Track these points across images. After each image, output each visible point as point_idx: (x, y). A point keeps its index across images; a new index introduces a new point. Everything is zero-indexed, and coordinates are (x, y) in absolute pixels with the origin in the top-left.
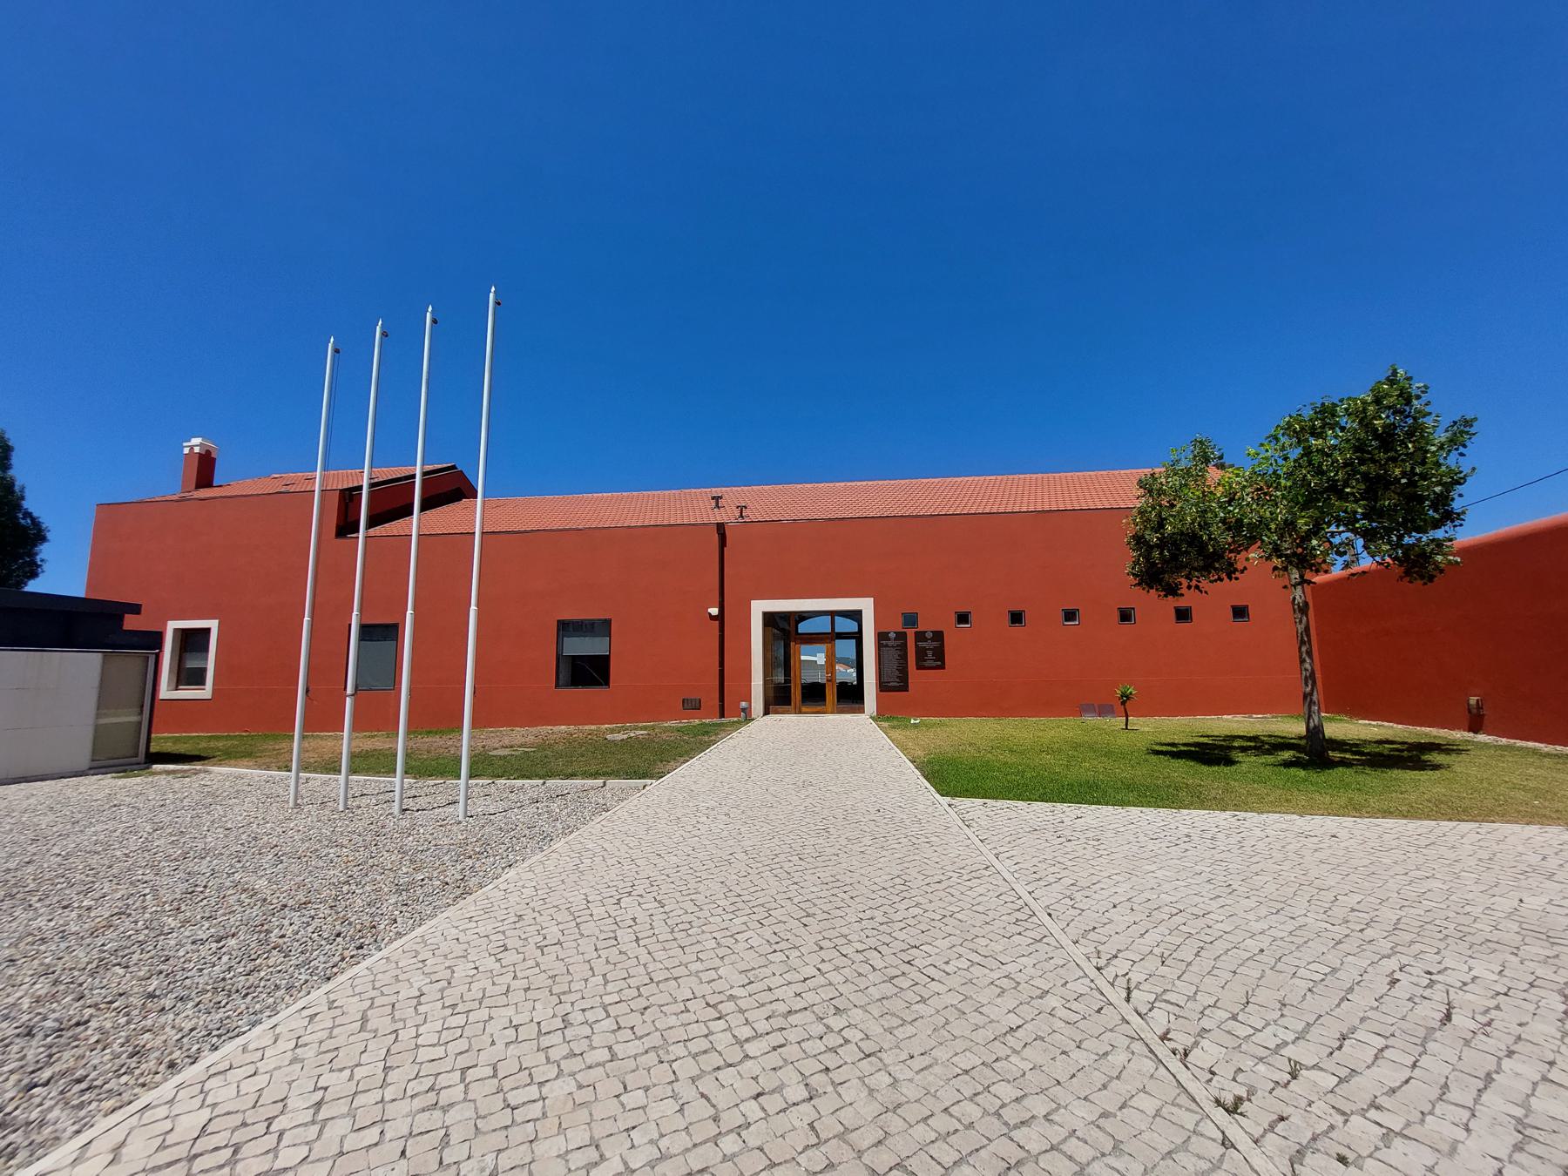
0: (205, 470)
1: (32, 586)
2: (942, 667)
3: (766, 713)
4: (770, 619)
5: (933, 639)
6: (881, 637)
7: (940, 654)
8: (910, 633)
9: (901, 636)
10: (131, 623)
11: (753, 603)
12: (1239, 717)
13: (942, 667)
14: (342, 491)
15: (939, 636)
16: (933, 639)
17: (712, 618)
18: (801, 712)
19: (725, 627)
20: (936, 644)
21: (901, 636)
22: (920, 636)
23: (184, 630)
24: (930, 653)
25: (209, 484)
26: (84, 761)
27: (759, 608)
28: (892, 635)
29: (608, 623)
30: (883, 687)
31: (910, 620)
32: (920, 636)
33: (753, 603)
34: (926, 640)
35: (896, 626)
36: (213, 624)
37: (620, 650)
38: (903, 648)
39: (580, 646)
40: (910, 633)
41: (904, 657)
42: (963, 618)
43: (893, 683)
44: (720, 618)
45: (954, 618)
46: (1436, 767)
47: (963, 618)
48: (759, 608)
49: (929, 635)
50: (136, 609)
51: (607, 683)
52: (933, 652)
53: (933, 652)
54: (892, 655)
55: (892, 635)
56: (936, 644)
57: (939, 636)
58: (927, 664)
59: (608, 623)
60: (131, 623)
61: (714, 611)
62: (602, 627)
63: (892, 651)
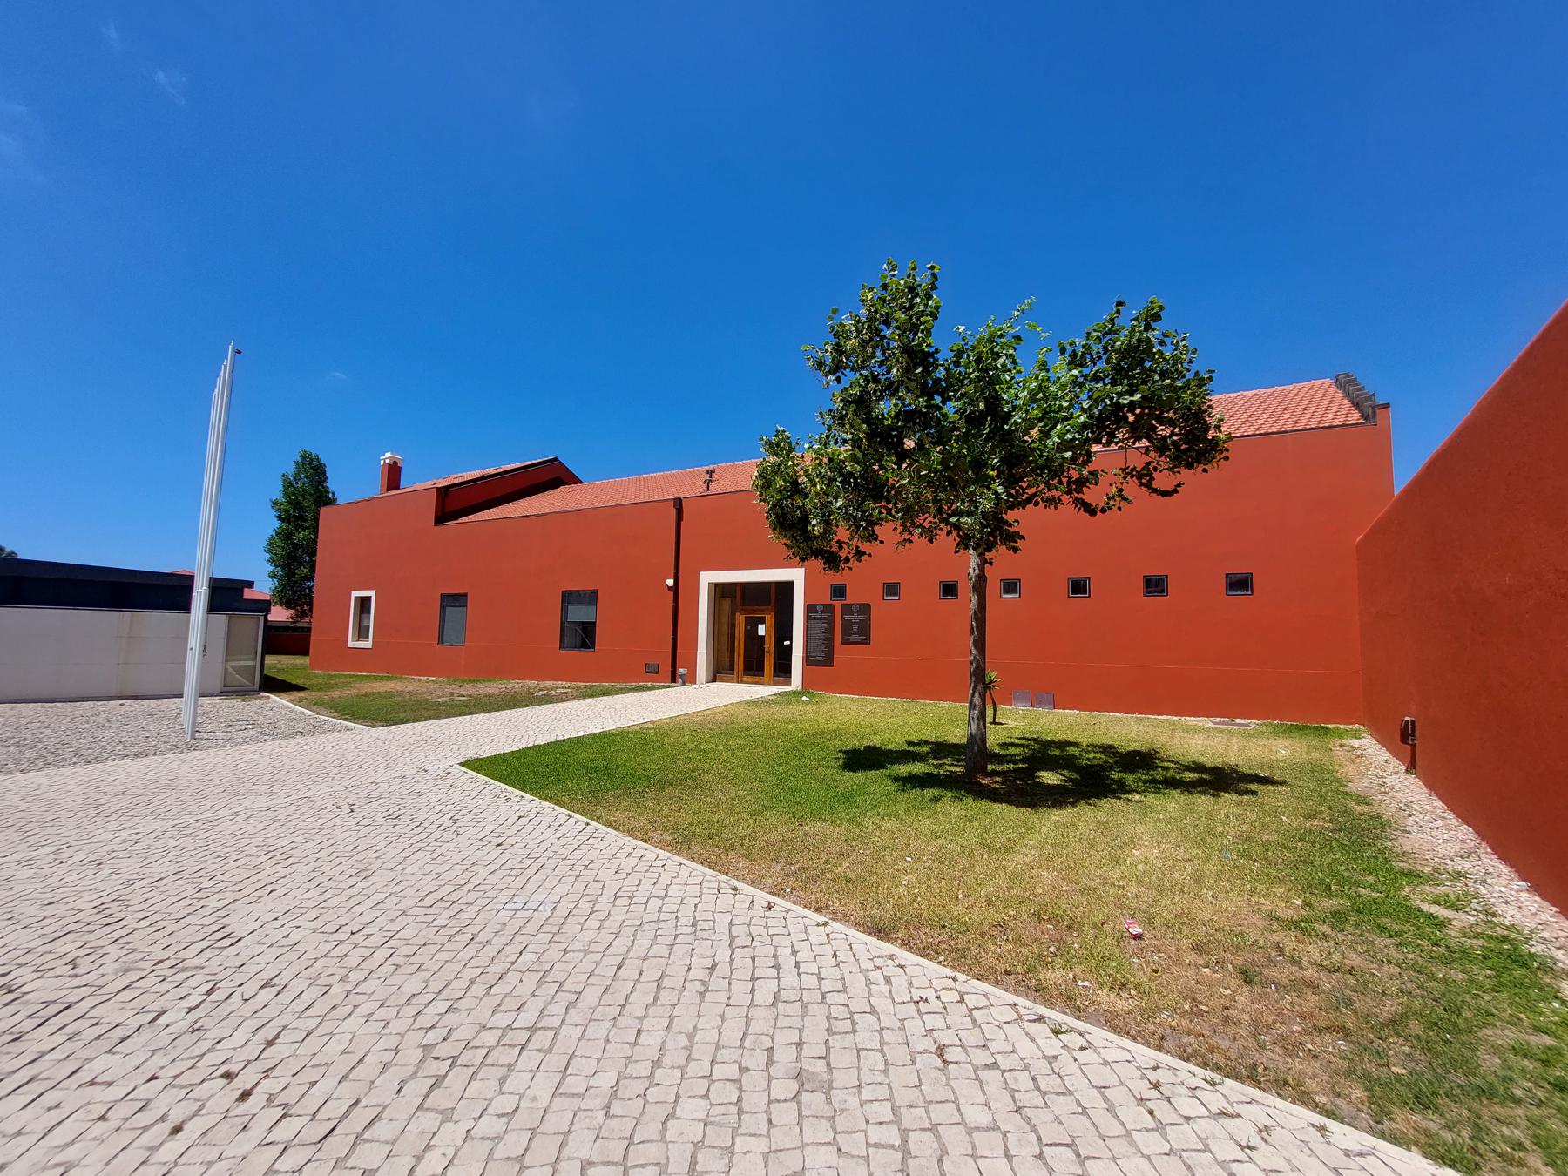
0: (393, 475)
1: (1396, 493)
6: (810, 609)
7: (865, 629)
9: (829, 609)
10: (248, 594)
12: (877, 702)
14: (439, 489)
15: (865, 609)
17: (670, 589)
19: (679, 597)
20: (862, 617)
21: (829, 609)
22: (847, 609)
23: (717, 585)
25: (398, 488)
26: (218, 687)
27: (707, 578)
29: (595, 592)
30: (809, 661)
32: (847, 609)
35: (826, 598)
36: (372, 593)
37: (604, 617)
38: (830, 621)
39: (578, 614)
41: (830, 630)
42: (892, 589)
43: (819, 659)
44: (675, 589)
46: (1254, 793)
47: (892, 589)
50: (250, 584)
52: (859, 628)
54: (819, 627)
56: (862, 617)
57: (865, 609)
58: (852, 638)
59: (595, 592)
60: (248, 594)
61: (670, 582)
62: (591, 598)
63: (820, 624)
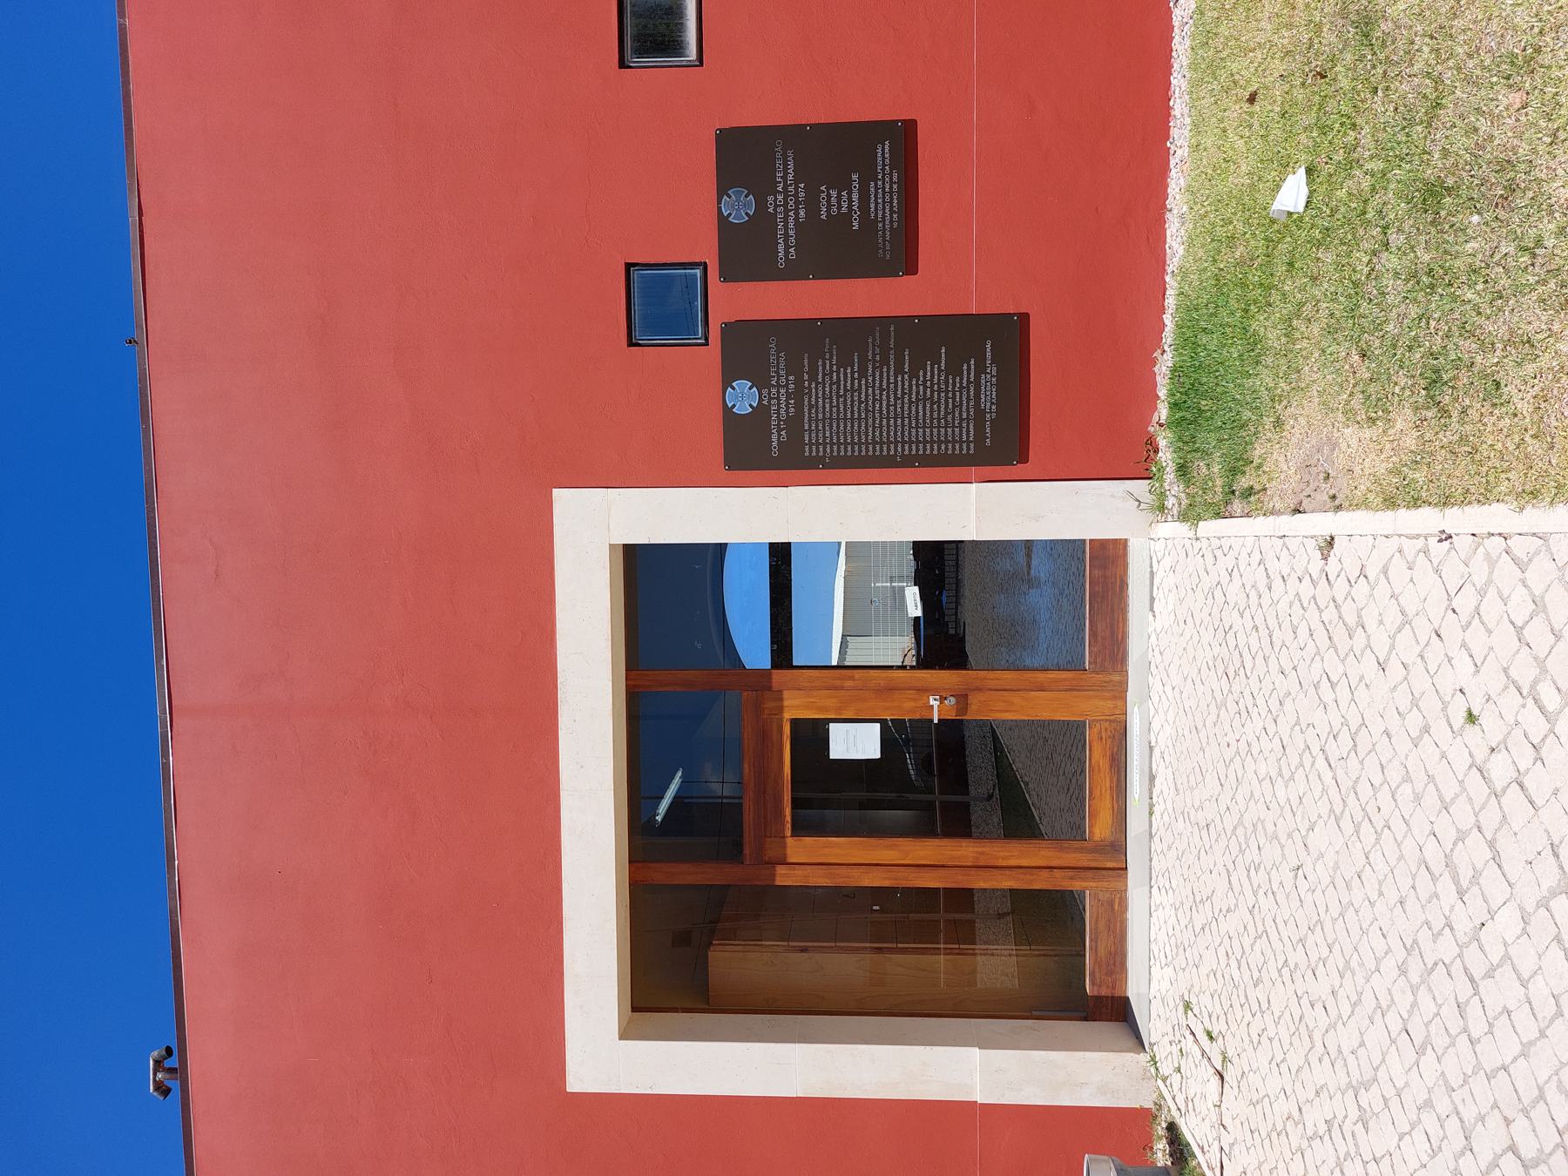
2: (904, 135)
3: (1114, 1012)
4: (673, 977)
5: (761, 187)
6: (752, 454)
8: (734, 301)
11: (878, 755)
13: (904, 135)
15: (743, 155)
16: (761, 187)
18: (1118, 847)
20: (786, 171)
21: (746, 349)
22: (745, 253)
24: (832, 201)
28: (743, 397)
30: (1003, 449)
31: (657, 305)
32: (745, 253)
33: (878, 755)
34: (762, 222)
40: (734, 301)
41: (850, 337)
45: (651, 75)
48: (604, 1052)
49: (740, 207)
51: (1024, 318)
52: (831, 184)
53: (831, 184)
55: (743, 397)
56: (786, 171)
57: (743, 155)
58: (885, 211)
